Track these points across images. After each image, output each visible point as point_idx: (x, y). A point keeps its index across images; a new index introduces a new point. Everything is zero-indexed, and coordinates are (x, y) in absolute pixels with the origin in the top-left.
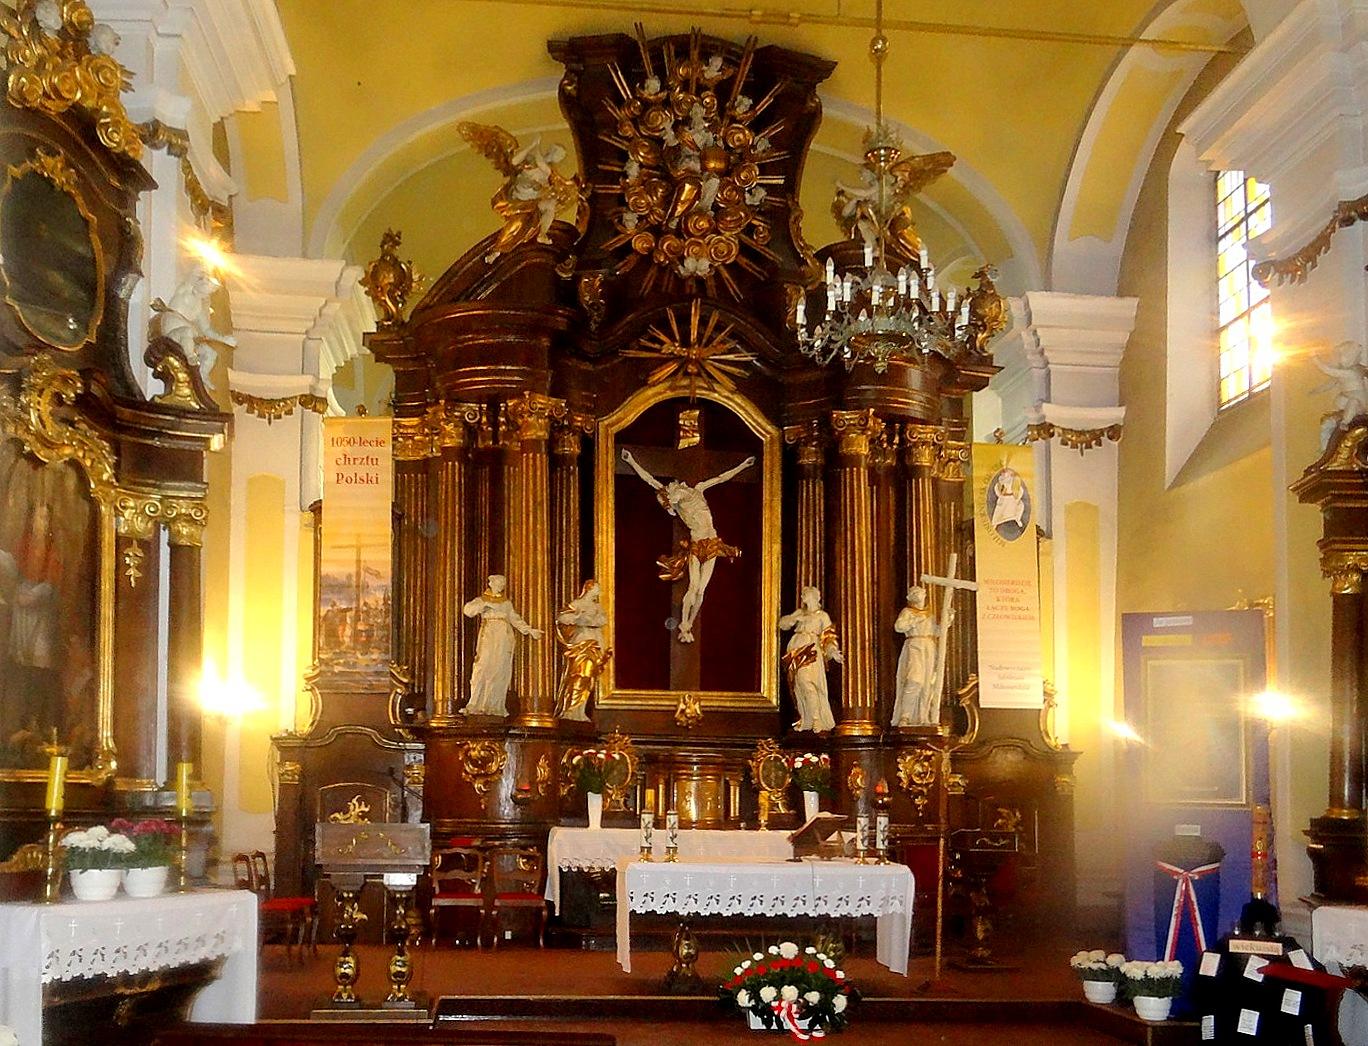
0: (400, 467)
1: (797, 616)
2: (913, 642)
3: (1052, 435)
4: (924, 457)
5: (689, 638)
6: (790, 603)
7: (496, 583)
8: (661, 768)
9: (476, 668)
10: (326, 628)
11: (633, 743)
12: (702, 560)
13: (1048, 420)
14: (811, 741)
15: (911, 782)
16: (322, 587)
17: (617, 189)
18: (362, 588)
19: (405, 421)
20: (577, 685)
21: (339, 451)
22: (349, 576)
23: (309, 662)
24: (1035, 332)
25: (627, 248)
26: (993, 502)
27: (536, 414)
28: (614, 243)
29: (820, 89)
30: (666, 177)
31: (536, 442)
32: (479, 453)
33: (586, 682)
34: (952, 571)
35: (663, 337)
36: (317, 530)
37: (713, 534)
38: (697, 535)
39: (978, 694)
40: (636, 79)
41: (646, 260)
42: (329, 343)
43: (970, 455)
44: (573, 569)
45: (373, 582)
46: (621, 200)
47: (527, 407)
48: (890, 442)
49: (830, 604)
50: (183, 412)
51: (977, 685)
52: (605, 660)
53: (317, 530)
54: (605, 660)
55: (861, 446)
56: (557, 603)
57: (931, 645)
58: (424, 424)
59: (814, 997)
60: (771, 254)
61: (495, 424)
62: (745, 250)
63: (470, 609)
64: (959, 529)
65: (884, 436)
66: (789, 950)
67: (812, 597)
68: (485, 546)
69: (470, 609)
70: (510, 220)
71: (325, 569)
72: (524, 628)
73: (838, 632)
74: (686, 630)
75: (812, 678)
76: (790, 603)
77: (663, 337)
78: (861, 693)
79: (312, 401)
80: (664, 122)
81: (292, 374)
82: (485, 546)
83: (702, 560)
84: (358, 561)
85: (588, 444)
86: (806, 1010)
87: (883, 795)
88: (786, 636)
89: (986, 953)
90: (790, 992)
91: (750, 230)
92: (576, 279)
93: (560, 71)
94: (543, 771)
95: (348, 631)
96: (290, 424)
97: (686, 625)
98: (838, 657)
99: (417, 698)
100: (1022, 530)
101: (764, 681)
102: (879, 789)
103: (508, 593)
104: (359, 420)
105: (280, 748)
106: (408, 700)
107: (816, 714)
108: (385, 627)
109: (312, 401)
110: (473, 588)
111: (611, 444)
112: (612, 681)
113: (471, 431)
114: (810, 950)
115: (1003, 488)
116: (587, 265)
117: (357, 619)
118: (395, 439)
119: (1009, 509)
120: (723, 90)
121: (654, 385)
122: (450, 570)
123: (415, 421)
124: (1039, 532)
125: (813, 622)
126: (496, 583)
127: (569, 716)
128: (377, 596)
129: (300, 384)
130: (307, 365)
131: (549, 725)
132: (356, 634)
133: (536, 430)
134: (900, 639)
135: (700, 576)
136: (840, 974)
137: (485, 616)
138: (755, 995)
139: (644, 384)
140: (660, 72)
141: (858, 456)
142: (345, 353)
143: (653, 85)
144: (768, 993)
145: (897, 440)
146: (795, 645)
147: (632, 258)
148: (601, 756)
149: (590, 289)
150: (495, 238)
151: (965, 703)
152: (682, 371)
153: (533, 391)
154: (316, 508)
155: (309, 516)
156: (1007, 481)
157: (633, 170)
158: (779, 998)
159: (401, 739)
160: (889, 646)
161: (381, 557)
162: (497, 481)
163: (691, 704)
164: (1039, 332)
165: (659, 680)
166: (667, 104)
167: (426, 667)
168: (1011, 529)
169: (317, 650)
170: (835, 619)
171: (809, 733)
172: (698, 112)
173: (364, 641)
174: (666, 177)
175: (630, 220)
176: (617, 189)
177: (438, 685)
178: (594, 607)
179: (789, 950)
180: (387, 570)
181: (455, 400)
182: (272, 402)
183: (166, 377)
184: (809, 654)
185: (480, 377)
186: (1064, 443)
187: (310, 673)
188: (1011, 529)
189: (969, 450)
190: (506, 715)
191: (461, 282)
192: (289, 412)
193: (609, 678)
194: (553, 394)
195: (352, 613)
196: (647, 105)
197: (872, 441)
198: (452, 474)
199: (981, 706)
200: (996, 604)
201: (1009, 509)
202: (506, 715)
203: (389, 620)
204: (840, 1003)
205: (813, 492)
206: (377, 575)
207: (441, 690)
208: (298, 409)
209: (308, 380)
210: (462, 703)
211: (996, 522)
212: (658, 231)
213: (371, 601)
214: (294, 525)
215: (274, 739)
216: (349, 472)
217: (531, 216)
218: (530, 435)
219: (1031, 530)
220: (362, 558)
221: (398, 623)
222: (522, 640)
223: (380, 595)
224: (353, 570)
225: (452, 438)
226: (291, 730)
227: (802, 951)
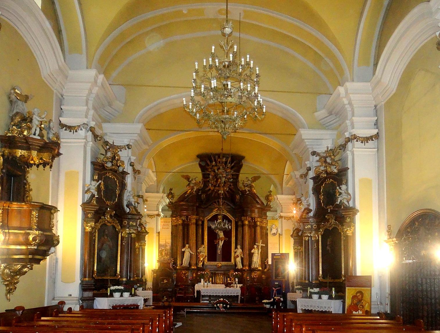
0: (172, 226)
1: (236, 250)
2: (254, 254)
3: (282, 218)
4: (258, 223)
5: (219, 253)
6: (236, 248)
7: (187, 245)
8: (214, 274)
9: (184, 259)
10: (160, 252)
11: (210, 270)
12: (221, 241)
13: (282, 215)
14: (238, 270)
15: (254, 277)
16: (160, 246)
17: (208, 179)
18: (166, 246)
19: (173, 218)
20: (200, 262)
21: (162, 224)
22: (164, 244)
23: (158, 258)
24: (279, 201)
25: (210, 189)
26: (271, 230)
27: (193, 219)
28: (207, 189)
29: (243, 161)
30: (216, 177)
31: (194, 223)
32: (185, 224)
33: (202, 261)
34: (261, 243)
35: (215, 204)
36: (159, 237)
37: (223, 236)
38: (221, 237)
39: (268, 262)
40: (211, 162)
41: (214, 190)
42: (161, 205)
43: (267, 222)
44: (200, 242)
45: (168, 245)
46: (209, 181)
47: (192, 218)
48: (252, 221)
49: (242, 248)
50: (143, 233)
51: (268, 261)
52: (205, 257)
53: (159, 237)
54: (205, 257)
55: (247, 223)
56: (197, 248)
57: (257, 255)
58: (176, 219)
59: (225, 305)
60: (234, 190)
61: (188, 220)
62: (229, 189)
63: (183, 250)
64: (266, 235)
65: (251, 220)
66: (222, 299)
67: (239, 247)
68: (186, 240)
69: (183, 250)
70: (189, 189)
71: (160, 243)
72: (191, 253)
73: (243, 252)
74: (219, 252)
75: (239, 260)
76: (236, 248)
77: (215, 204)
78: (246, 263)
79: (158, 215)
80: (216, 168)
81: (155, 211)
82: (186, 240)
83: (221, 241)
84: (166, 242)
85: (203, 222)
86: (223, 307)
87: (248, 279)
88: (235, 252)
89: (258, 302)
90: (221, 305)
91: (230, 185)
92: (201, 195)
93: (199, 160)
94: (194, 275)
95: (164, 253)
96: (155, 219)
97: (219, 251)
98: (243, 257)
99: (175, 263)
100: (276, 234)
101: (232, 260)
102: (247, 278)
103: (189, 247)
104: (165, 218)
105: (153, 272)
106: (173, 264)
107: (240, 266)
108: (169, 252)
109: (158, 215)
110: (184, 246)
111: (207, 221)
112: (207, 261)
113: (183, 221)
114: (225, 299)
115: (273, 227)
116: (203, 193)
117: (165, 251)
118: (172, 221)
119: (274, 231)
120: (226, 163)
121: (214, 212)
122: (180, 244)
123: (175, 218)
124: (279, 234)
125: (239, 251)
126: (187, 245)
127: (199, 266)
128: (169, 247)
129: (156, 213)
130: (158, 210)
131: (195, 268)
132: (165, 253)
133: (194, 221)
134: (253, 253)
135: (221, 243)
136: (229, 303)
137: (185, 251)
138: (217, 305)
139: (212, 212)
140: (215, 161)
141: (246, 224)
142: (163, 205)
143: (214, 163)
144: (218, 305)
145: (253, 221)
146: (237, 254)
147: (211, 191)
148: (203, 273)
149: (204, 196)
150: (186, 193)
151: (266, 263)
152: (219, 209)
153: (193, 215)
154: (159, 233)
155: (158, 234)
156: (274, 226)
157: (211, 177)
158: (220, 305)
159: (172, 270)
160: (251, 255)
161: (169, 241)
162: (188, 230)
163: (220, 264)
164: (280, 201)
165: (215, 260)
166: (216, 165)
167: (177, 258)
168: (274, 234)
169: (159, 256)
170: (243, 250)
171: (238, 269)
172: (221, 167)
173: (166, 254)
174: (216, 177)
175: (210, 185)
176: (208, 179)
177: (178, 261)
178: (203, 249)
179: (222, 299)
180: (170, 243)
181: (181, 216)
182: (152, 215)
183: (141, 228)
184: (238, 256)
185: (185, 213)
186: (285, 219)
187: (158, 260)
188: (274, 234)
189: (267, 221)
190: (189, 266)
191: (183, 198)
192: (155, 217)
193: (206, 260)
194: (196, 215)
195: (165, 250)
196: (213, 166)
197: (249, 222)
198: (181, 227)
199: (269, 264)
200: (272, 247)
201: (274, 231)
202: (189, 266)
203: (171, 251)
204: (228, 306)
205: (240, 229)
206: (169, 244)
207: (179, 262)
208: (156, 216)
209: (158, 212)
210: (182, 264)
211: (272, 233)
212: (215, 186)
213: (168, 248)
214: (155, 235)
215: (152, 270)
216: (164, 227)
217: (192, 189)
218: (192, 222)
219: (278, 234)
220: (166, 241)
221: (172, 251)
222: (191, 255)
223: (169, 247)
224: (165, 243)
225: (180, 222)
226: (155, 269)
227: (224, 299)
